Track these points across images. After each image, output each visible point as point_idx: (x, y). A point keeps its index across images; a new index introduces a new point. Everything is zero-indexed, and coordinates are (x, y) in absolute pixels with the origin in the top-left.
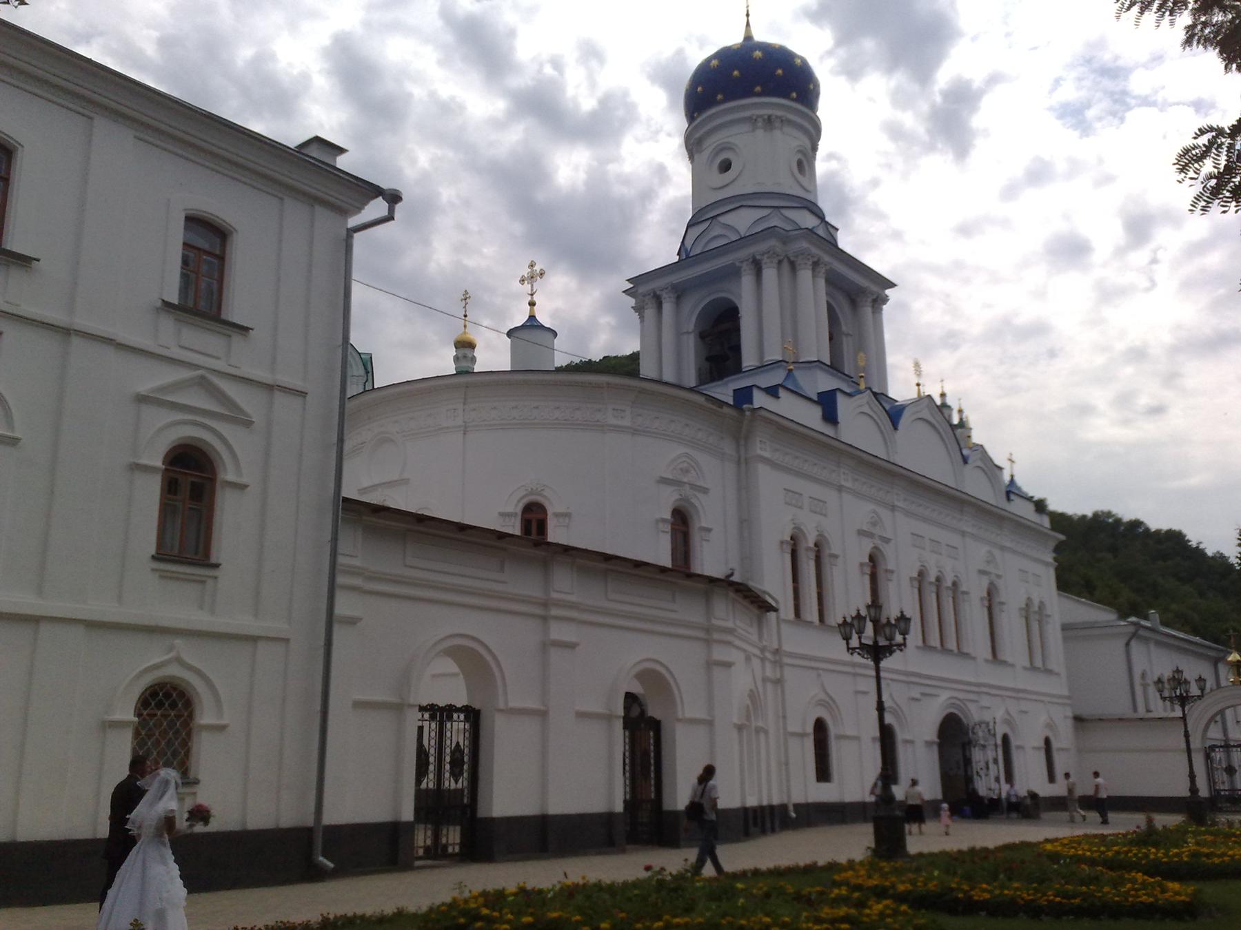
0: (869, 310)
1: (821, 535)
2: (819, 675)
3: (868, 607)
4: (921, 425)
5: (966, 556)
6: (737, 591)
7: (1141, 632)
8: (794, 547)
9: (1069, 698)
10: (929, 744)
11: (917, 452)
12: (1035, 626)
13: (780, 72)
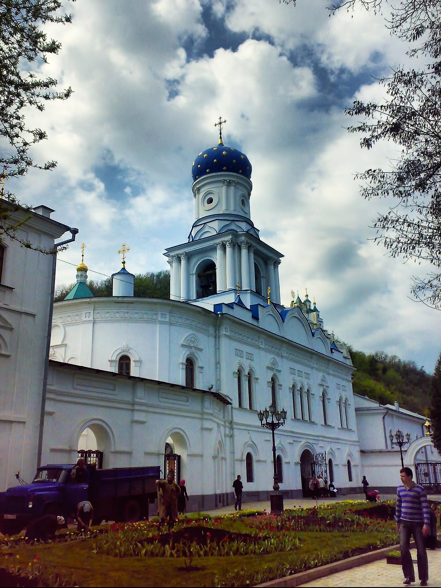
0: (273, 267)
1: (251, 369)
2: (250, 435)
3: (271, 407)
4: (295, 319)
5: (314, 379)
6: (215, 396)
7: (390, 412)
8: (239, 374)
9: (358, 442)
10: (296, 464)
11: (294, 332)
12: (343, 409)
13: (234, 161)
